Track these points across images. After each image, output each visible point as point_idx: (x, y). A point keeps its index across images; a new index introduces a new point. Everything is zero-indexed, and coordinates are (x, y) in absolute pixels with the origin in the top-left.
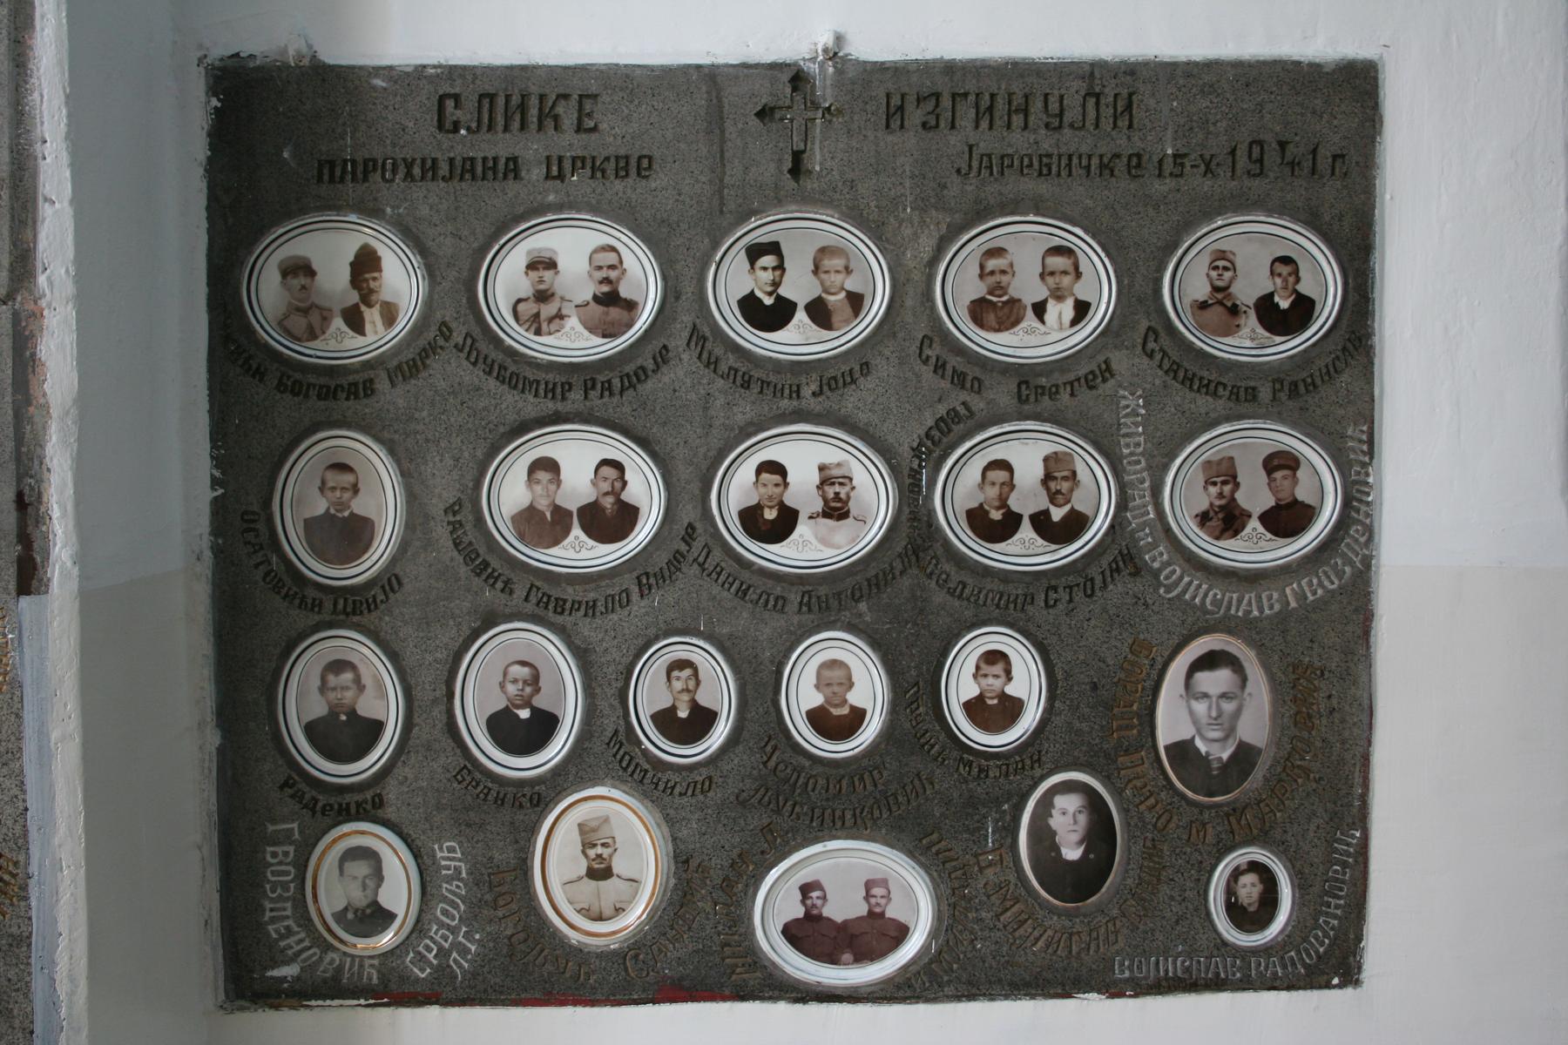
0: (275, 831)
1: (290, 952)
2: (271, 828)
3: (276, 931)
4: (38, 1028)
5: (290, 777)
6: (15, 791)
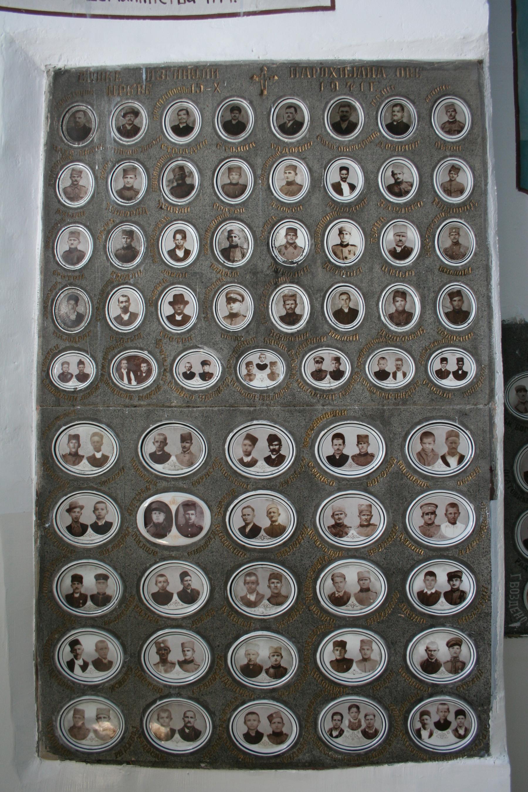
0: (513, 577)
1: (517, 618)
2: (512, 576)
3: (513, 611)
4: (492, 643)
5: (519, 559)
6: (488, 565)
